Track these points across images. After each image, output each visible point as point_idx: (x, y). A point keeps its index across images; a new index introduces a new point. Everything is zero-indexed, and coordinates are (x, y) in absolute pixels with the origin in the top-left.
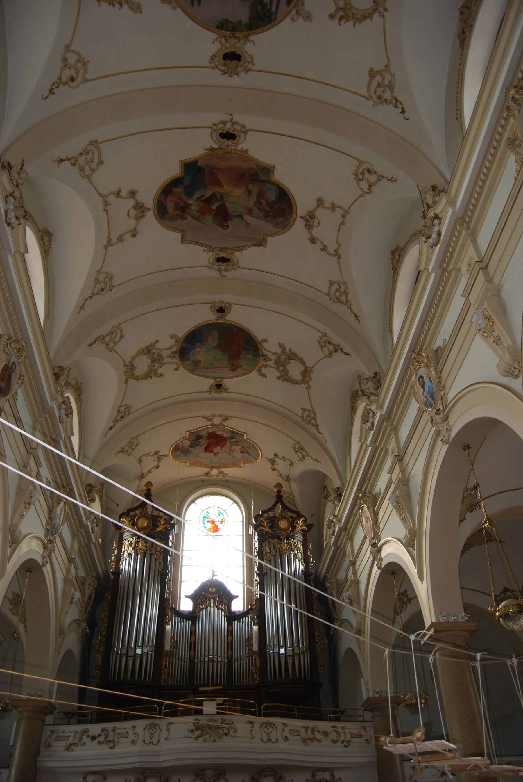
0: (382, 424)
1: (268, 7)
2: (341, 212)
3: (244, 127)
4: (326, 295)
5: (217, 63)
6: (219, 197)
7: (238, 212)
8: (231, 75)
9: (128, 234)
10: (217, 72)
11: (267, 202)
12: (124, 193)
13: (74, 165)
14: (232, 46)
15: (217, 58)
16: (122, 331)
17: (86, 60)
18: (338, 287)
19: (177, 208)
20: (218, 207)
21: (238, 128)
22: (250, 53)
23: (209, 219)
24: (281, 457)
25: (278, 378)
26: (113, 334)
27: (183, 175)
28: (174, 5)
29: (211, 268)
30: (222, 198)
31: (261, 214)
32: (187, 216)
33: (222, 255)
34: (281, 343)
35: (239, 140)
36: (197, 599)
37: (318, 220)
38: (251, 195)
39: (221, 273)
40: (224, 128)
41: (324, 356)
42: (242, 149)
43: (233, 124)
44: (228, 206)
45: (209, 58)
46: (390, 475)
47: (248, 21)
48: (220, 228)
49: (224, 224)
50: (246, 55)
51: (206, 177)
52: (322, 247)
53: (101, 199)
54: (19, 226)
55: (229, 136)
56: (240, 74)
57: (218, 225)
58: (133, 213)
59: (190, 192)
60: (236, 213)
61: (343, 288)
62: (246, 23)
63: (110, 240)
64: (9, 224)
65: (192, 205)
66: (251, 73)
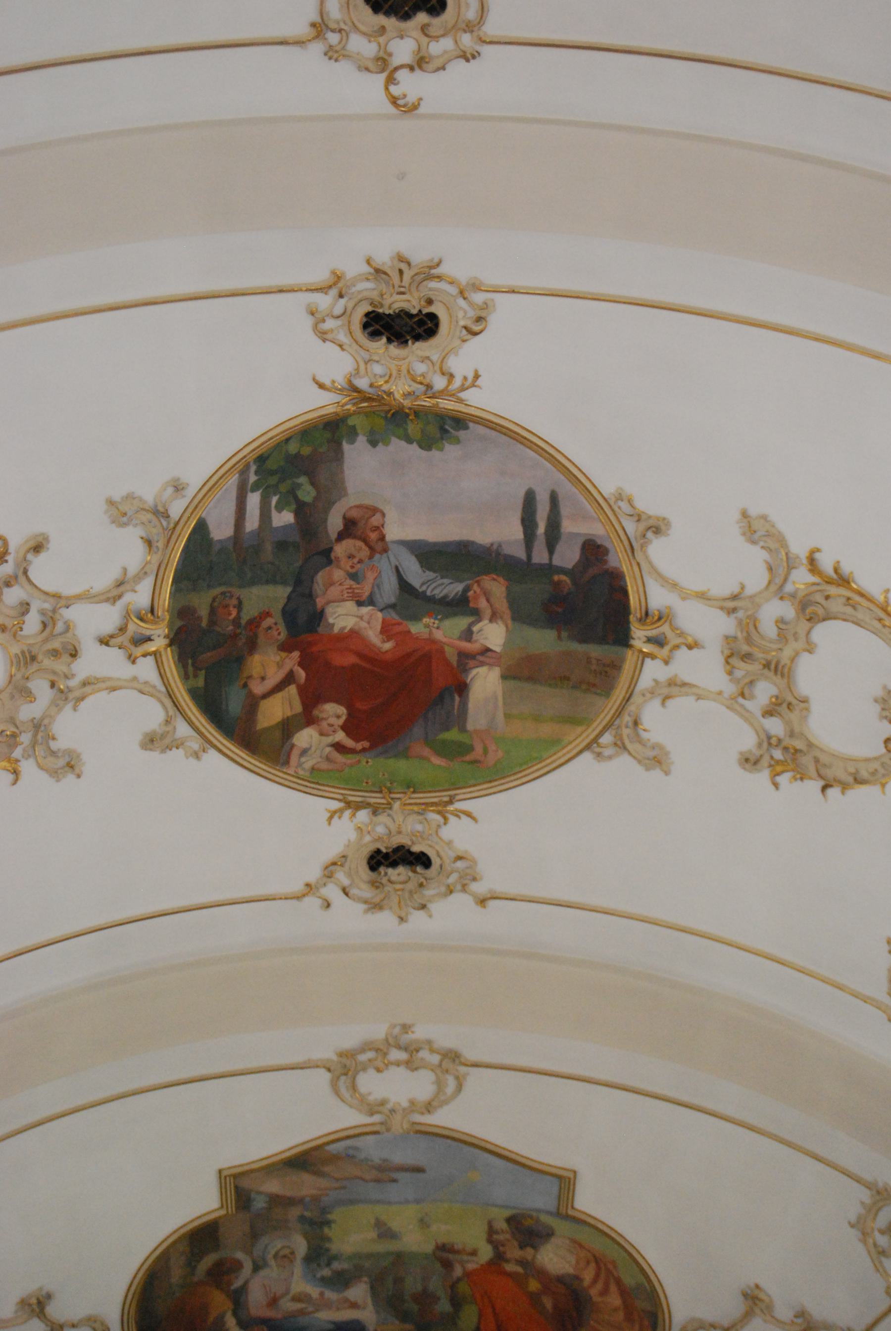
1: (274, 500)
3: (333, 54)
5: (461, 302)
8: (403, 266)
15: (462, 323)
25: (749, 762)
34: (657, 774)
36: (465, 402)
39: (394, 89)
40: (425, 40)
45: (494, 320)
47: (346, 446)
50: (343, 337)
62: (352, 441)
66: (321, 276)
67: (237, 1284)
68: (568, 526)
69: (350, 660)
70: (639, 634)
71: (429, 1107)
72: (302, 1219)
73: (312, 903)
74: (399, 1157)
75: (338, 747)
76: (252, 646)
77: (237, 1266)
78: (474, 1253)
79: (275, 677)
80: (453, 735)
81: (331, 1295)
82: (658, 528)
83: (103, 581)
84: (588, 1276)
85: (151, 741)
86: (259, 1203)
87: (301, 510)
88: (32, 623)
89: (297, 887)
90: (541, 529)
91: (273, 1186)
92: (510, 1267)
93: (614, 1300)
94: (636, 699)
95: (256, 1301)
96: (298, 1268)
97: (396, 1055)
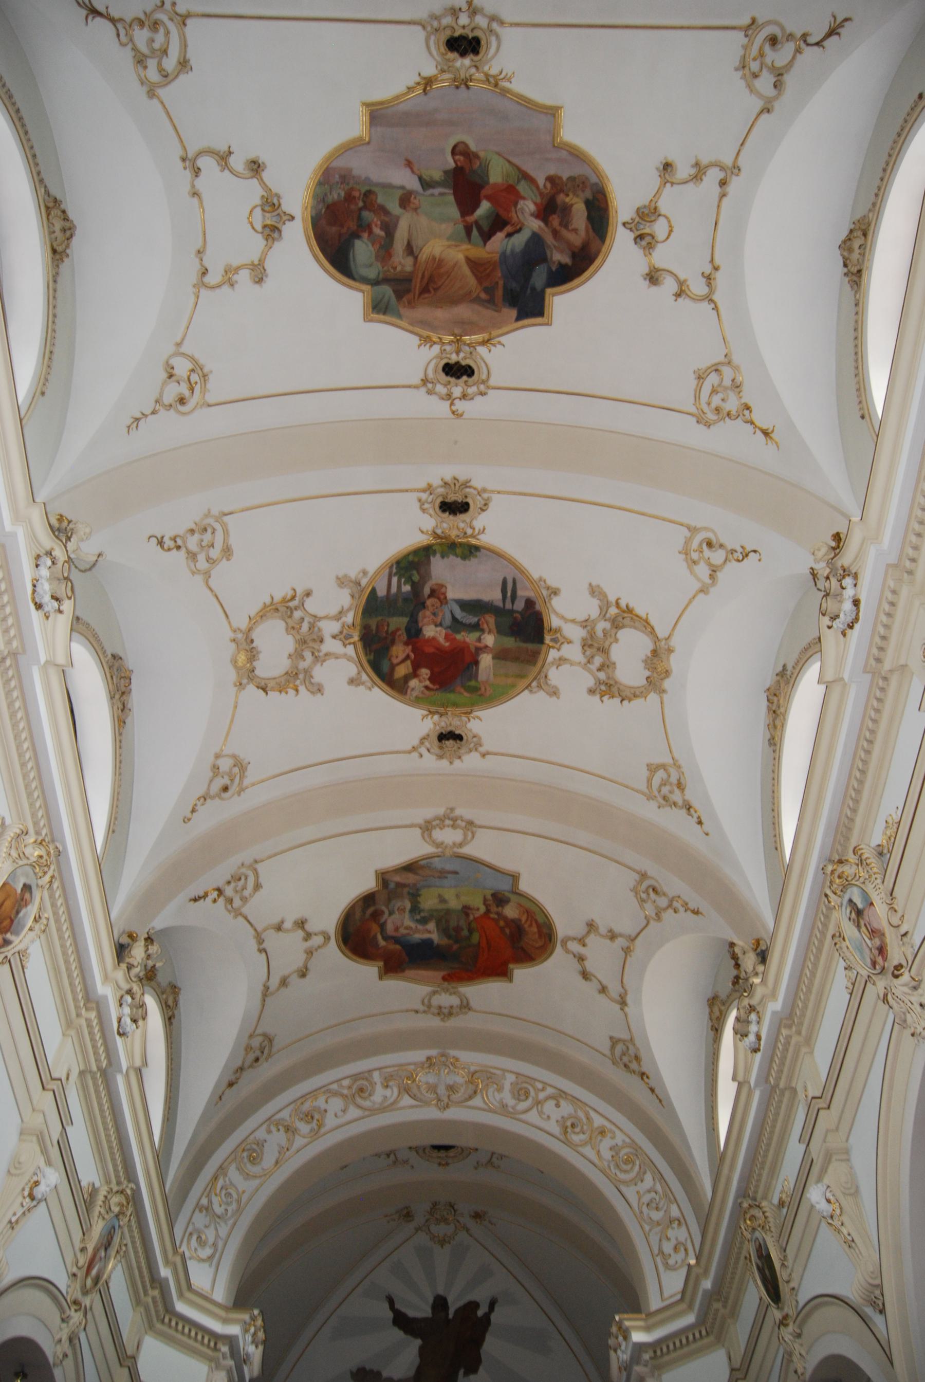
0: (779, 1032)
1: (403, 580)
2: (213, 278)
3: (430, 392)
4: (189, 15)
5: (478, 497)
6: (475, 232)
7: (432, 195)
9: (296, 974)
10: (477, 483)
11: (371, 232)
12: (288, 925)
13: (748, 408)
14: (453, 526)
15: (479, 506)
16: (256, 871)
17: (740, 73)
19: (566, 210)
20: (476, 205)
21: (441, 389)
22: (426, 516)
23: (496, 176)
24: (603, 930)
25: (591, 691)
26: (240, 879)
27: (549, 291)
28: (542, 583)
29: (493, 18)
30: (468, 230)
31: (380, 200)
32: (545, 185)
33: (467, 61)
35: (436, 367)
37: (253, 228)
38: (406, 243)
40: (465, 388)
41: (697, 586)
42: (431, 346)
43: (449, 396)
44: (454, 211)
45: (492, 505)
46: (803, 1147)
47: (431, 558)
48: (473, 147)
49: (462, 158)
50: (431, 511)
51: (501, 283)
52: (232, 160)
53: (715, 297)
54: (59, 615)
55: (456, 371)
56: (441, 483)
57: (476, 156)
58: (659, 228)
59: (536, 247)
60: (436, 191)
61: (632, 1051)
63: (723, 183)
64: (39, 606)
65: (532, 215)
66: (423, 485)
67: (382, 921)
68: (520, 593)
69: (432, 650)
70: (547, 639)
71: (461, 845)
72: (409, 893)
73: (415, 754)
74: (449, 867)
75: (427, 687)
76: (393, 642)
77: (383, 913)
78: (478, 909)
79: (402, 656)
81: (420, 927)
82: (555, 592)
83: (334, 611)
84: (524, 919)
85: (352, 681)
86: (392, 886)
87: (414, 585)
88: (305, 626)
89: (409, 747)
90: (509, 594)
91: (397, 878)
92: (493, 916)
93: (535, 929)
95: (390, 927)
96: (407, 915)
97: (448, 822)
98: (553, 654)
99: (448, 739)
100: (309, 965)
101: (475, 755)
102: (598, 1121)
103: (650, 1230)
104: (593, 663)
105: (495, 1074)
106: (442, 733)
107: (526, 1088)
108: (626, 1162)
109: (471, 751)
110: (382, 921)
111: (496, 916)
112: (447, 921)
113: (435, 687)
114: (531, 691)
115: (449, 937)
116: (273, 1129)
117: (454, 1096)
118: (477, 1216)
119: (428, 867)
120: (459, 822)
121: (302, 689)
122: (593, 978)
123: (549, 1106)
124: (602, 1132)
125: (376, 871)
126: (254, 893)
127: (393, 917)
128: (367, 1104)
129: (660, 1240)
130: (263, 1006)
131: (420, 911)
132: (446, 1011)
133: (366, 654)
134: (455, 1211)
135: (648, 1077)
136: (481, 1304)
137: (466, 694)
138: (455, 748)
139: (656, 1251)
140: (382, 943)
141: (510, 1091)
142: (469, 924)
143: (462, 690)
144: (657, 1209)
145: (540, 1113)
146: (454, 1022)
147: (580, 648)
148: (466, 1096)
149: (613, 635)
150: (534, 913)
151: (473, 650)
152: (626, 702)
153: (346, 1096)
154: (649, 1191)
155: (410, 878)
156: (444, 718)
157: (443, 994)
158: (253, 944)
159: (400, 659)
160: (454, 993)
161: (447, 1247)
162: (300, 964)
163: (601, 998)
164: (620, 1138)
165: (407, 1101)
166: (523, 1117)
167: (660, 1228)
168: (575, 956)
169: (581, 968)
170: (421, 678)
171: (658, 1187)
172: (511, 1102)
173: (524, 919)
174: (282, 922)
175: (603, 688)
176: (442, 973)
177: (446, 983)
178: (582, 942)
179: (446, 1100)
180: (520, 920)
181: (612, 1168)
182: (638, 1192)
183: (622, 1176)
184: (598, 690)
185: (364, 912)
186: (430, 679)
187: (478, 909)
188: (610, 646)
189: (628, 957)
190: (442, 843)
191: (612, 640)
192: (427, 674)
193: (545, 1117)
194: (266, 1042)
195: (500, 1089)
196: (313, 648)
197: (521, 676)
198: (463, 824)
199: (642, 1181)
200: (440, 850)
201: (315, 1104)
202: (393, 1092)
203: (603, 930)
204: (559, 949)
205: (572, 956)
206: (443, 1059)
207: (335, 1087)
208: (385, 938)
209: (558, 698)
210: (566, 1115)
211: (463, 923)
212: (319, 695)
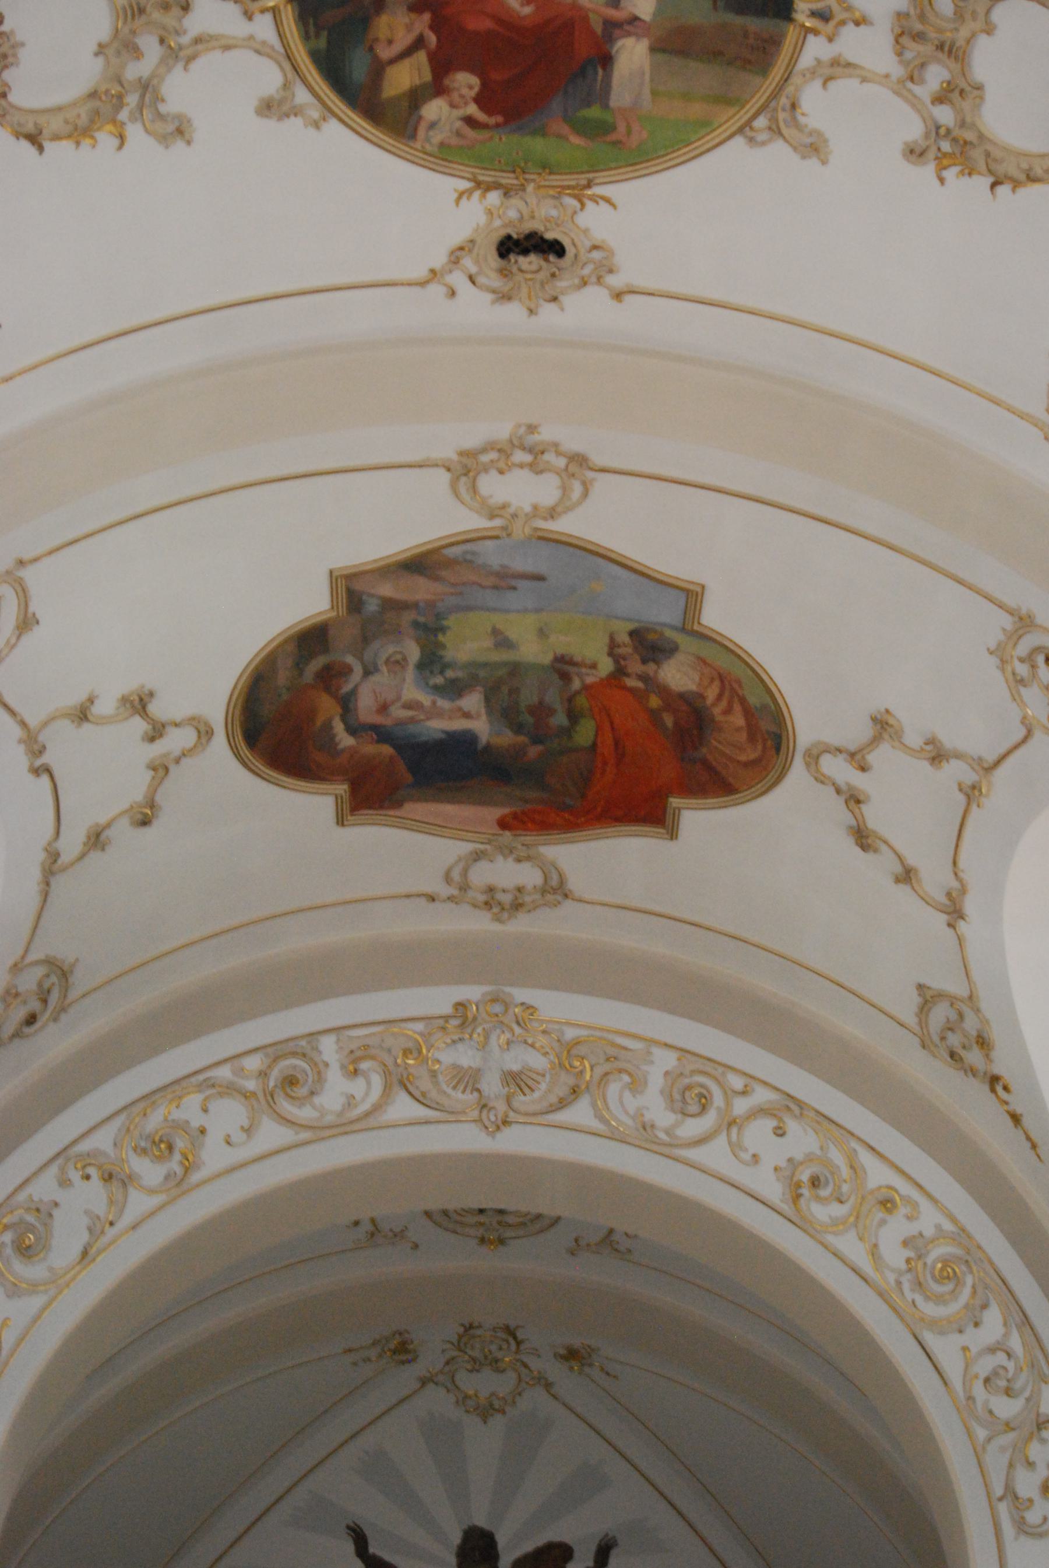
9: (125, 822)
12: (105, 706)
16: (23, 593)
18: (953, 1016)
24: (913, 739)
25: (914, 153)
61: (971, 1024)
67: (347, 688)
71: (552, 513)
72: (416, 624)
73: (436, 290)
74: (519, 565)
75: (470, 121)
77: (348, 670)
78: (594, 666)
79: (403, 40)
80: (594, 112)
81: (443, 703)
84: (711, 694)
85: (268, 108)
86: (372, 606)
89: (421, 273)
91: (387, 590)
92: (631, 682)
94: (796, 80)
95: (365, 706)
96: (410, 673)
98: (815, 49)
99: (525, 252)
100: (158, 798)
101: (594, 297)
102: (878, 1175)
103: (989, 1440)
104: (922, 81)
105: (625, 1048)
106: (509, 237)
107: (702, 1086)
108: (942, 1278)
109: (584, 283)
110: (347, 688)
111: (640, 685)
112: (514, 691)
113: (492, 121)
114: (751, 140)
115: (518, 728)
116: (75, 1176)
117: (522, 1098)
118: (572, 1355)
119: (467, 562)
120: (549, 457)
121: (134, 132)
122: (884, 848)
123: (759, 1133)
124: (887, 1204)
125: (331, 572)
126: (19, 637)
127: (375, 678)
128: (305, 1113)
129: (1011, 1465)
130: (45, 895)
131: (445, 667)
132: (506, 899)
133: (306, 37)
134: (518, 1343)
135: (1006, 1088)
136: (576, 1548)
137: (575, 140)
138: (542, 276)
139: (999, 1491)
140: (345, 740)
141: (662, 1092)
142: (570, 700)
143: (565, 129)
144: (1009, 1392)
145: (736, 1148)
146: (521, 925)
147: (891, 39)
148: (553, 1099)
149: (981, 16)
150: (739, 682)
151: (598, 29)
152: (1003, 190)
153: (254, 1094)
154: (992, 1350)
155: (421, 589)
156: (515, 201)
157: (500, 859)
158: (20, 758)
159: (398, 47)
160: (529, 858)
161: (498, 1422)
162: (138, 795)
163: (903, 892)
164: (929, 1221)
165: (403, 1107)
166: (692, 1154)
167: (1011, 1436)
168: (838, 791)
169: (854, 823)
170: (455, 96)
171: (1015, 1343)
172: (662, 1116)
173: (711, 694)
174: (91, 700)
175: (946, 146)
176: (498, 812)
177: (507, 833)
178: (858, 759)
179: (501, 1107)
180: (702, 697)
181: (906, 1286)
182: (965, 1349)
183: (930, 1309)
184: (932, 154)
185: (299, 666)
186: (477, 100)
187: (594, 666)
188: (968, 42)
189: (974, 807)
190: (504, 507)
191: (979, 25)
192: (471, 87)
193: (746, 1156)
194: (54, 979)
195: (637, 1085)
196: (164, 28)
197: (727, 100)
198: (562, 462)
199: (976, 1325)
200: (497, 522)
201: (177, 1115)
202: (369, 1083)
203: (913, 739)
204: (797, 774)
205: (832, 790)
206: (498, 1008)
207: (224, 1073)
208: (352, 730)
209: (824, 162)
210: (799, 1156)
211: (553, 697)
212: (180, 145)
